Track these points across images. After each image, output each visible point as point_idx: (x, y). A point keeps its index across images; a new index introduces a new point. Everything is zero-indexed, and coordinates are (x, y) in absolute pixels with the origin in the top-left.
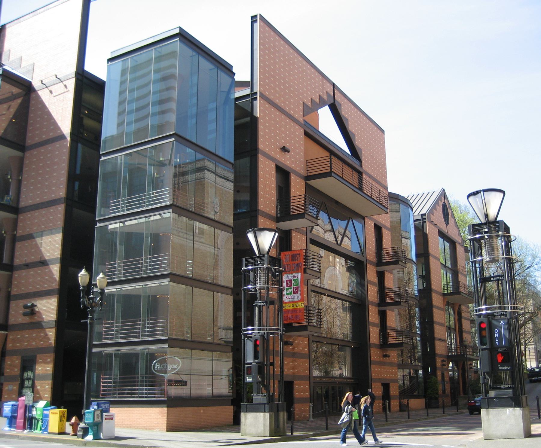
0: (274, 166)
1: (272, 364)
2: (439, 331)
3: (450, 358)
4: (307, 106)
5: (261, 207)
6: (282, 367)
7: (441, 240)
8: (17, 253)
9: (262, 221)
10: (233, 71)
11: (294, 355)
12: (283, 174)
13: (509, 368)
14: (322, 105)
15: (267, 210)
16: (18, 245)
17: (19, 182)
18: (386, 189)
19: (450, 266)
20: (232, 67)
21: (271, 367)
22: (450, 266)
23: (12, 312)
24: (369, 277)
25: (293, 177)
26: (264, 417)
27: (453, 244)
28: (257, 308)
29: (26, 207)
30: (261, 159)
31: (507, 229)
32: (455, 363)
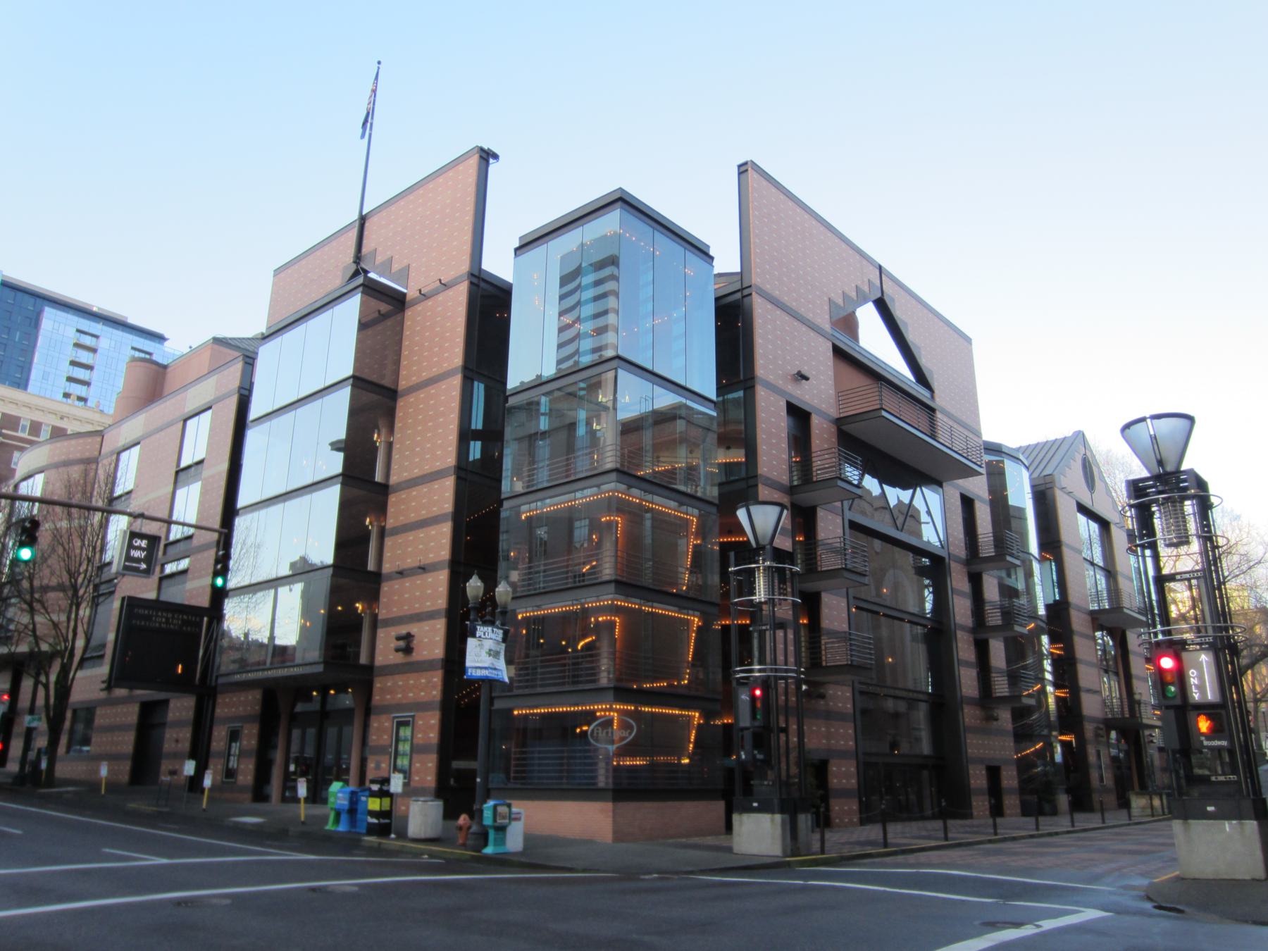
0: (783, 404)
1: (785, 730)
2: (1087, 675)
3: (1109, 724)
4: (837, 305)
5: (763, 469)
6: (801, 735)
7: (1082, 519)
8: (387, 554)
9: (764, 492)
10: (711, 253)
11: (829, 715)
12: (799, 415)
13: (1224, 743)
14: (862, 300)
15: (774, 475)
16: (388, 542)
17: (390, 446)
18: (978, 435)
19: (1101, 564)
20: (708, 247)
21: (783, 737)
22: (1101, 564)
23: (380, 645)
24: (954, 583)
25: (815, 420)
26: (772, 821)
27: (1104, 525)
28: (756, 635)
29: (399, 484)
30: (761, 392)
31: (1201, 485)
32: (1123, 733)
